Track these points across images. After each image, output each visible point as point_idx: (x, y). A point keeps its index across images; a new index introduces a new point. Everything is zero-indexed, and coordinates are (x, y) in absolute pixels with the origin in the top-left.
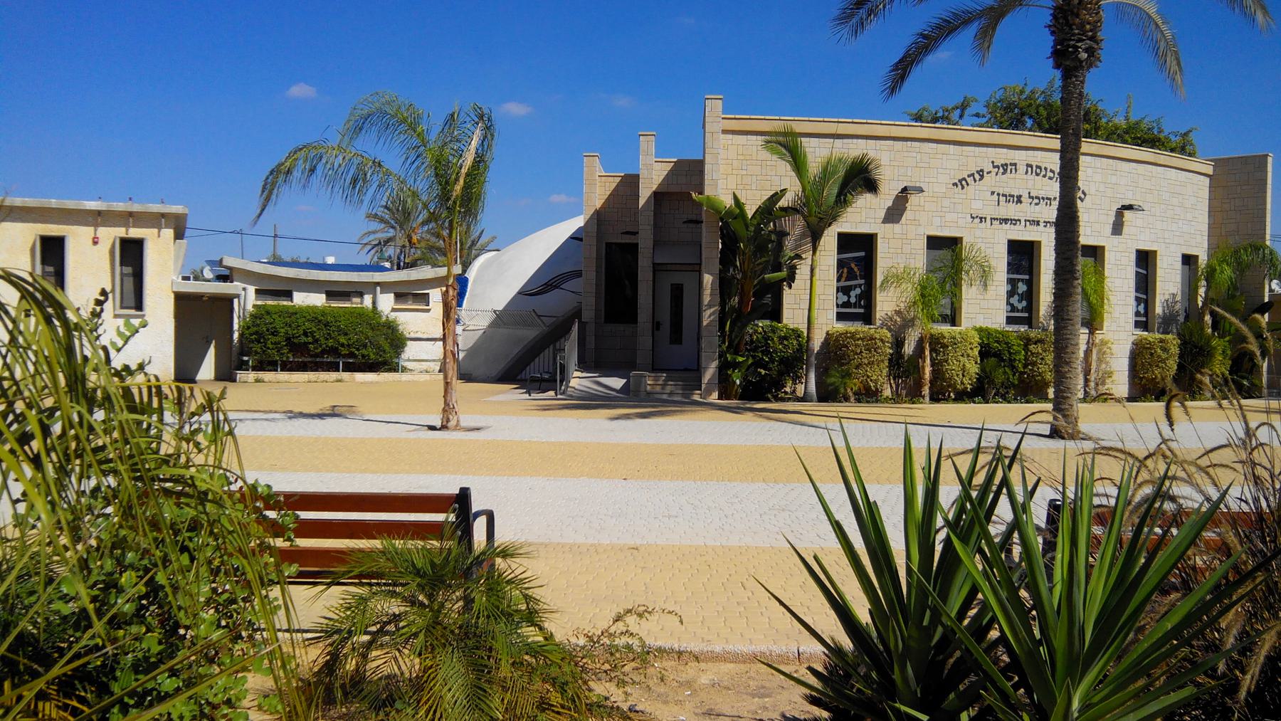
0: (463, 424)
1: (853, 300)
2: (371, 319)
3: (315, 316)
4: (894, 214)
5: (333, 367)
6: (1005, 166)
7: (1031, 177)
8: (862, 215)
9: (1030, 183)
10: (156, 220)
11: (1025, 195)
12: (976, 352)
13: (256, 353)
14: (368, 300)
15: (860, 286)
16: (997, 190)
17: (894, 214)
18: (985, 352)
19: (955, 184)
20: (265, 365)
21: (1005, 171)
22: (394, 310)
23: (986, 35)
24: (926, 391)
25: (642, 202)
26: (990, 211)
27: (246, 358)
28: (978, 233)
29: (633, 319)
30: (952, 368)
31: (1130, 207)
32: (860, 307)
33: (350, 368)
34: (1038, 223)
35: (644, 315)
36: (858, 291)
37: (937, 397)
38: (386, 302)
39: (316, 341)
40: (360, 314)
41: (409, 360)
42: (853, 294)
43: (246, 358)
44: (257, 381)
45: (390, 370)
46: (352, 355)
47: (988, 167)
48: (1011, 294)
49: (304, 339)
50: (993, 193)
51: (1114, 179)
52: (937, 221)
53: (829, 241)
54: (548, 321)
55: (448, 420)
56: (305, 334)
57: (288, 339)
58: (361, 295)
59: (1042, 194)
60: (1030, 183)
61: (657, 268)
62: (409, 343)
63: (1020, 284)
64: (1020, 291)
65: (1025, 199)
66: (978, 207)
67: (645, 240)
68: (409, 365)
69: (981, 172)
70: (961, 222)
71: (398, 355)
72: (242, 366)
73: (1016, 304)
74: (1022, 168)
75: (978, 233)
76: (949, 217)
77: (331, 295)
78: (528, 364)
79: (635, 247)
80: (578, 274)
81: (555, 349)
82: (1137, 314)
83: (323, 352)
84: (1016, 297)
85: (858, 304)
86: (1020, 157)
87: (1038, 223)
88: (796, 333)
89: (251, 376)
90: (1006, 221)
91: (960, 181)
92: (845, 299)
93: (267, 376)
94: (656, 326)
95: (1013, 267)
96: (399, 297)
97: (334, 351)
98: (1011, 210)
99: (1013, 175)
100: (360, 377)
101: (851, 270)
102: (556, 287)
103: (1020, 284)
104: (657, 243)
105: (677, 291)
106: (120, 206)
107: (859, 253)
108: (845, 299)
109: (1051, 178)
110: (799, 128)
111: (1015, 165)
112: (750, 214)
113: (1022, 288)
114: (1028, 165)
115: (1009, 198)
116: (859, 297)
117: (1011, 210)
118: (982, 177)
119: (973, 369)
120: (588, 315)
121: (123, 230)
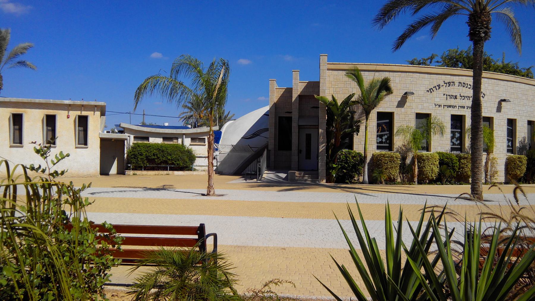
1: (384, 140)
3: (158, 148)
4: (402, 103)
5: (165, 169)
6: (449, 83)
8: (387, 104)
9: (461, 91)
10: (93, 108)
11: (458, 95)
13: (134, 163)
14: (180, 141)
15: (387, 134)
16: (446, 93)
17: (402, 103)
18: (442, 163)
19: (428, 91)
20: (137, 168)
22: (190, 145)
23: (435, 29)
24: (416, 179)
25: (293, 99)
27: (129, 165)
28: (438, 112)
29: (289, 148)
32: (387, 143)
33: (172, 169)
36: (386, 137)
38: (187, 142)
39: (158, 158)
40: (177, 147)
41: (197, 166)
42: (384, 138)
43: (129, 165)
44: (134, 174)
45: (188, 170)
46: (173, 164)
47: (442, 83)
48: (452, 138)
49: (153, 157)
50: (444, 95)
52: (420, 107)
53: (373, 115)
56: (154, 155)
57: (147, 157)
58: (177, 139)
59: (465, 95)
61: (300, 127)
62: (197, 159)
63: (457, 133)
65: (458, 97)
66: (438, 101)
67: (295, 116)
69: (439, 86)
70: (431, 107)
71: (192, 163)
72: (128, 168)
74: (457, 84)
77: (165, 139)
80: (266, 130)
83: (161, 163)
84: (455, 139)
86: (456, 79)
89: (131, 172)
90: (450, 106)
91: (430, 89)
92: (380, 140)
93: (138, 172)
95: (453, 126)
96: (193, 139)
97: (166, 162)
98: (452, 102)
99: (453, 87)
100: (176, 173)
101: (383, 128)
102: (258, 135)
103: (457, 133)
104: (300, 117)
106: (78, 102)
108: (380, 140)
110: (360, 67)
111: (454, 82)
113: (457, 135)
114: (459, 83)
115: (451, 96)
116: (386, 139)
117: (452, 102)
118: (439, 88)
119: (436, 170)
121: (80, 112)
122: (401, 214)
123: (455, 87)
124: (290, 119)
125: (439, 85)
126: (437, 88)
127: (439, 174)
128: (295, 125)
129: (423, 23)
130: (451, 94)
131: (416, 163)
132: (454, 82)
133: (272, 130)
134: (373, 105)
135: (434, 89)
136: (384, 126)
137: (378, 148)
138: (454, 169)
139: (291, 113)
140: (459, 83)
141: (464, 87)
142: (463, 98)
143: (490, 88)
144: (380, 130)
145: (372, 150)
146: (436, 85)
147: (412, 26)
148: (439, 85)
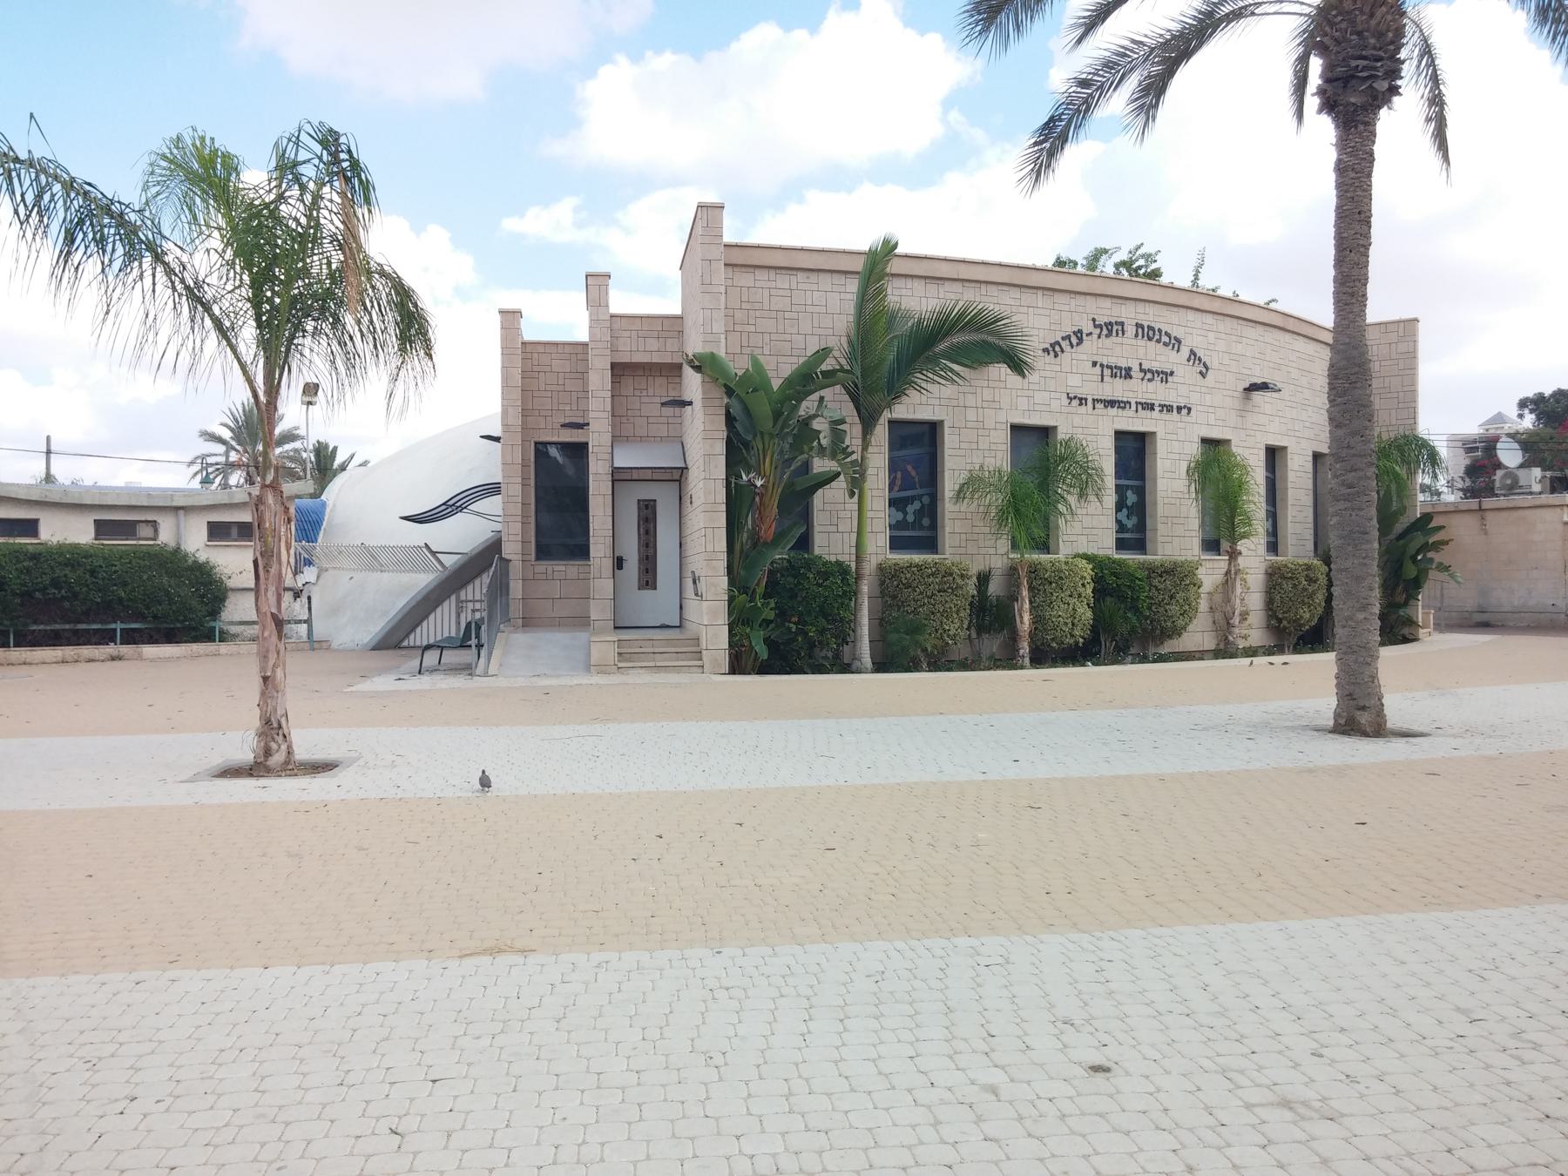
0: (301, 754)
1: (910, 518)
2: (174, 562)
3: (71, 556)
6: (1109, 325)
7: (1141, 342)
9: (1141, 351)
11: (1136, 368)
12: (1089, 591)
15: (920, 497)
16: (1099, 359)
18: (1102, 589)
19: (1046, 350)
21: (1110, 332)
23: (1153, 92)
24: (1025, 648)
26: (1092, 389)
28: (1077, 420)
29: (581, 551)
30: (1058, 613)
31: (1264, 387)
32: (921, 527)
34: (1151, 407)
35: (599, 547)
36: (917, 505)
37: (1040, 658)
41: (232, 623)
42: (910, 509)
47: (1087, 327)
48: (1120, 506)
50: (1094, 364)
51: (1239, 349)
52: (1023, 403)
53: (881, 433)
54: (449, 561)
55: (268, 752)
59: (1155, 366)
60: (1141, 351)
61: (619, 477)
63: (1129, 493)
64: (1129, 503)
65: (1136, 373)
66: (1076, 384)
67: (598, 437)
68: (234, 629)
69: (1079, 334)
70: (1055, 405)
71: (215, 613)
73: (1125, 521)
75: (1077, 420)
76: (1040, 397)
78: (419, 623)
79: (583, 447)
80: (492, 489)
81: (458, 601)
82: (1121, 528)
84: (1125, 511)
85: (917, 520)
87: (1151, 407)
88: (842, 569)
90: (1111, 403)
91: (1052, 345)
92: (900, 516)
94: (619, 563)
95: (1121, 470)
96: (218, 531)
98: (1116, 389)
99: (1119, 340)
101: (905, 474)
102: (460, 509)
103: (1129, 493)
104: (617, 439)
105: (647, 515)
107: (920, 446)
108: (900, 516)
109: (1166, 344)
111: (1122, 324)
112: (776, 384)
113: (1131, 498)
114: (1137, 325)
116: (919, 514)
117: (1116, 389)
118: (1080, 340)
119: (1086, 614)
120: (511, 550)
122: (1422, 735)
123: (1125, 341)
124: (578, 451)
125: (1080, 331)
126: (1074, 340)
127: (1095, 629)
128: (598, 470)
129: (1087, 94)
130: (1113, 361)
131: (1025, 593)
132: (1122, 324)
133: (516, 489)
134: (895, 388)
135: (1064, 344)
136: (909, 468)
137: (896, 544)
138: (1136, 610)
139: (581, 426)
140: (1137, 325)
141: (1150, 339)
142: (1149, 376)
143: (1221, 346)
144: (898, 482)
145: (878, 548)
146: (1069, 330)
147: (1084, 83)
148: (1080, 331)
